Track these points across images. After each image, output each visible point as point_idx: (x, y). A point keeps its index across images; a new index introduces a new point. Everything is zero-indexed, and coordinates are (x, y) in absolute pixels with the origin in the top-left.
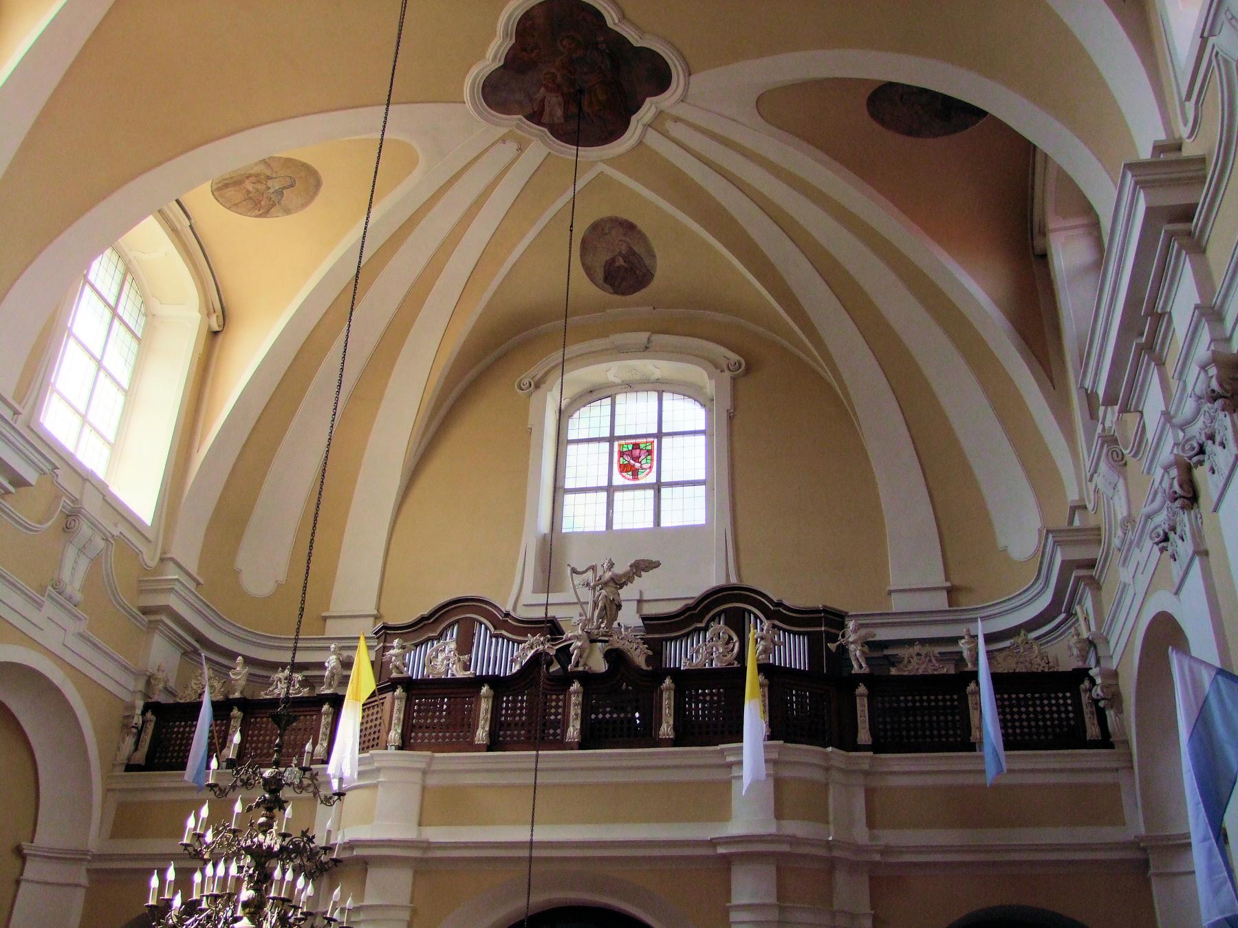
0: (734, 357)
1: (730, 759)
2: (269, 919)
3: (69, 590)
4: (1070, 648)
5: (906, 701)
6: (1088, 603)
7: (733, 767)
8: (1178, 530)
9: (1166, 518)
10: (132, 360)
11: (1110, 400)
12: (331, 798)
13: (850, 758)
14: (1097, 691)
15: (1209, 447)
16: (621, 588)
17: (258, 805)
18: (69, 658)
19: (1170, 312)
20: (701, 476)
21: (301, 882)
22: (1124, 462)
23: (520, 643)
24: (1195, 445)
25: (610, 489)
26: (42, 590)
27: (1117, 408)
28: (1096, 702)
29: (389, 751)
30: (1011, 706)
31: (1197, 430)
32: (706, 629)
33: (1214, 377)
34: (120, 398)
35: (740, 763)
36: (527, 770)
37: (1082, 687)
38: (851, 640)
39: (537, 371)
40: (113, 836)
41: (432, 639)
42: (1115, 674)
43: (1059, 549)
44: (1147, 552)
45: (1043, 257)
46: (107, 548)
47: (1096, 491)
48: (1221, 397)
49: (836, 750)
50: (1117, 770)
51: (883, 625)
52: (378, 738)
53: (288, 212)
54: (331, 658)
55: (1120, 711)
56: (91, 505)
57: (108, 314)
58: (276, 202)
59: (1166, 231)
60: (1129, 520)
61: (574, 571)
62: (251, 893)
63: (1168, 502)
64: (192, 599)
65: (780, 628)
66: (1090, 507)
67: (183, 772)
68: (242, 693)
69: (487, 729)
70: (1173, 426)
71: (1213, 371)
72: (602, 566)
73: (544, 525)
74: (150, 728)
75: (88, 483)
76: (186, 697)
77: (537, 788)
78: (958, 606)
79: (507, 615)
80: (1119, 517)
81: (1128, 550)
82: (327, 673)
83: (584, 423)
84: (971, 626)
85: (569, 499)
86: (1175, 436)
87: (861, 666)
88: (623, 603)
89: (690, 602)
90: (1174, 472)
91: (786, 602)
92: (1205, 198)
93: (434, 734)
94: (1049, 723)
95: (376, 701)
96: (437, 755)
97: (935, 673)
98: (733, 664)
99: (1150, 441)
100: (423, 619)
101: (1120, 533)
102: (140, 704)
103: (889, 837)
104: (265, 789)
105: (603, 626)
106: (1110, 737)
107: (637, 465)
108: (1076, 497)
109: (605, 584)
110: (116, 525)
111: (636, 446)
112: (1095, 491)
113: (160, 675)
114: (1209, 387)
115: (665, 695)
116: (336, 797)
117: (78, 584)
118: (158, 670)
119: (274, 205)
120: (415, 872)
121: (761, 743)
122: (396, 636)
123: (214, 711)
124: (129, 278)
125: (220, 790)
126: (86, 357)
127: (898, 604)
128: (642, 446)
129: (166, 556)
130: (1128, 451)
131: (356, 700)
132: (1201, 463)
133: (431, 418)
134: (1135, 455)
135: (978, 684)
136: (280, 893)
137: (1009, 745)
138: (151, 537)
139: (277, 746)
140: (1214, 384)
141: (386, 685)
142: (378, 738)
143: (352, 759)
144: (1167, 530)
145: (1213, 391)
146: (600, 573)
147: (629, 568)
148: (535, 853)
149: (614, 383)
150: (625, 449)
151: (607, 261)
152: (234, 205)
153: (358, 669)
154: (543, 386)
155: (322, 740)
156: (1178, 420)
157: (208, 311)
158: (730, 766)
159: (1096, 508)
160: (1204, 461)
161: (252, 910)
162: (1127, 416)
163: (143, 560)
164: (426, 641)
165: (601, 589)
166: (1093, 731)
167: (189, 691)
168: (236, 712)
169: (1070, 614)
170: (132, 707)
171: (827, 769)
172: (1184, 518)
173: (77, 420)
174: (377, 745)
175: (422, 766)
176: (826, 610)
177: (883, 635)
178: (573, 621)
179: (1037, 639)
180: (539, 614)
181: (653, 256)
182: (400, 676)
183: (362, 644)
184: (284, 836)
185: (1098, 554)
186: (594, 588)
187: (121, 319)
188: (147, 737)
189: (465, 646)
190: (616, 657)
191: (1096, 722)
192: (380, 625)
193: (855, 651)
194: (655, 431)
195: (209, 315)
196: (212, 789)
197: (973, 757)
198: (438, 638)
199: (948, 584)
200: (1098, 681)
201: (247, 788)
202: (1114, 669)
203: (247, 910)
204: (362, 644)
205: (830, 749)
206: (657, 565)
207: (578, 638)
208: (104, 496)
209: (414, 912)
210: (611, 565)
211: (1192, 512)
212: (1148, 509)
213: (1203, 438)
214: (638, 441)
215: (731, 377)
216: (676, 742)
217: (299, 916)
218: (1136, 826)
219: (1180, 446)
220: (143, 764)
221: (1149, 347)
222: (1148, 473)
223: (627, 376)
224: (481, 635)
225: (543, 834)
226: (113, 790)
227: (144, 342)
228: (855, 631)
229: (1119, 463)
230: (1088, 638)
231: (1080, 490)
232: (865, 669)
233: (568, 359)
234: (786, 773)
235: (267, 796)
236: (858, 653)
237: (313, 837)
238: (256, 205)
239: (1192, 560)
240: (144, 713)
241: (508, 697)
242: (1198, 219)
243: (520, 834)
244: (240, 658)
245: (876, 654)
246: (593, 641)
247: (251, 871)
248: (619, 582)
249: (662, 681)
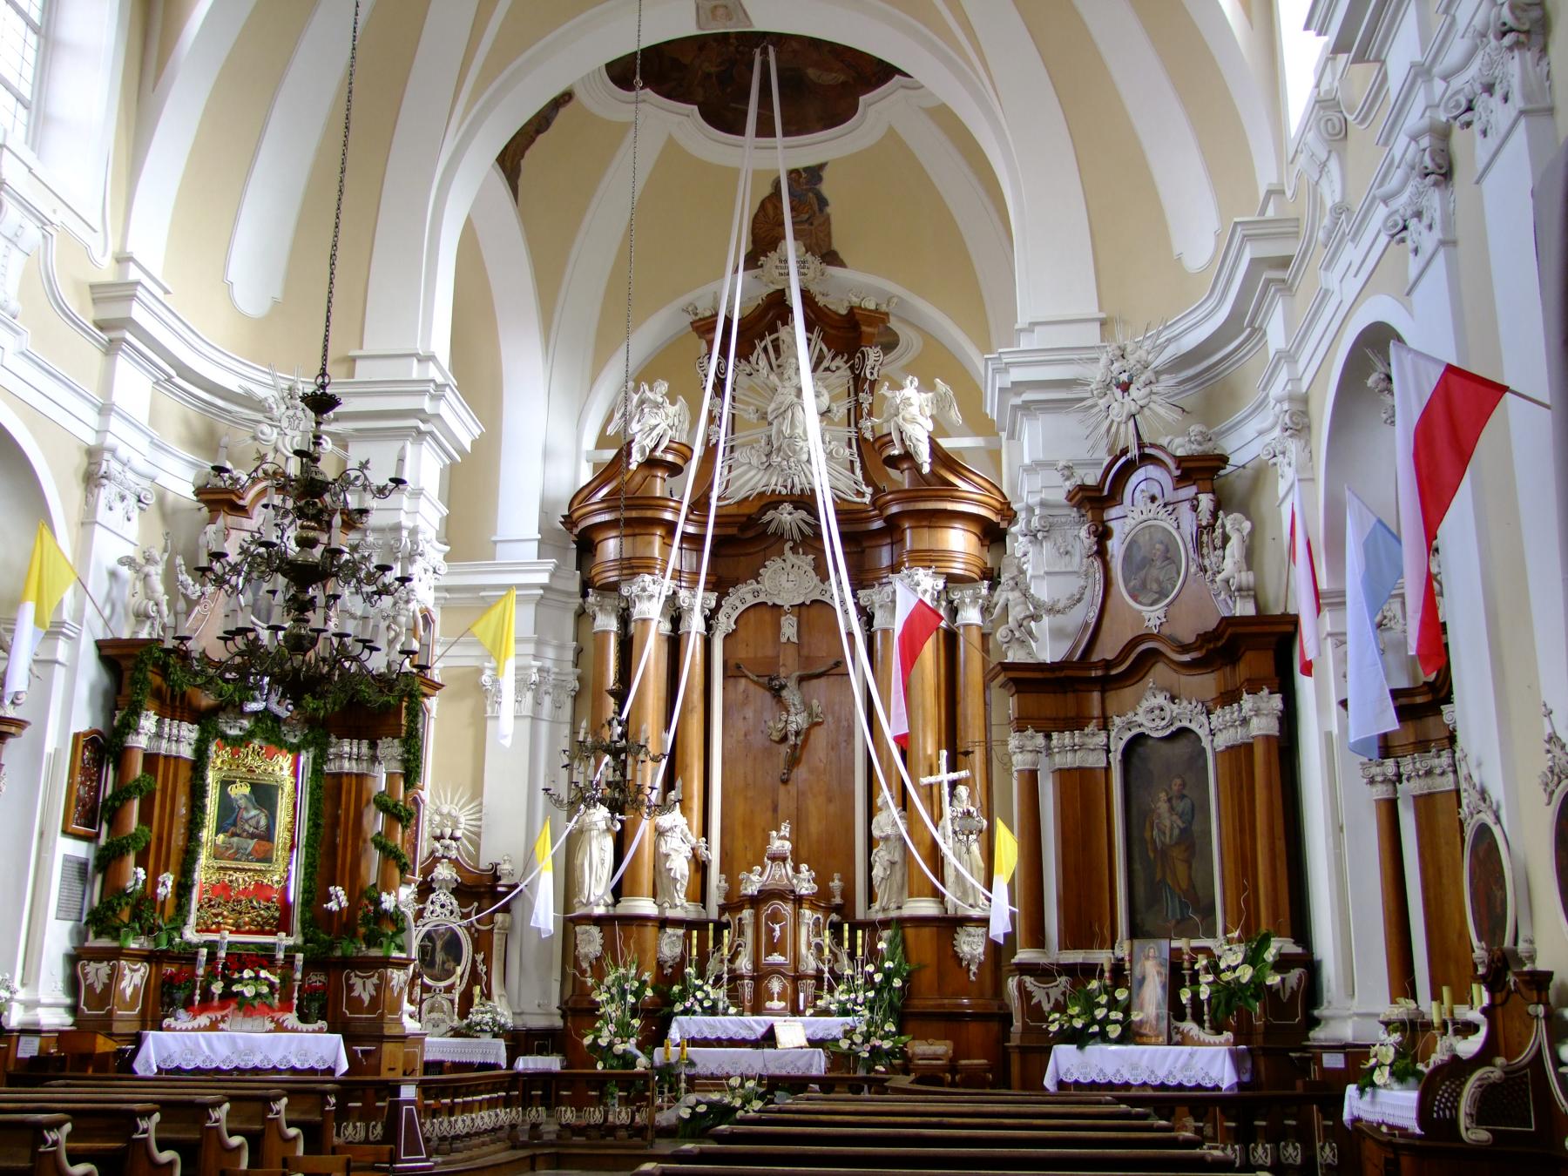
60: (1341, 210)
66: (1289, 194)
80: (1329, 204)
86: (1429, 92)
99: (1393, 101)
108: (1275, 181)
114: (1499, 18)
145: (1504, 24)
172: (1434, 200)
199: (1103, 315)
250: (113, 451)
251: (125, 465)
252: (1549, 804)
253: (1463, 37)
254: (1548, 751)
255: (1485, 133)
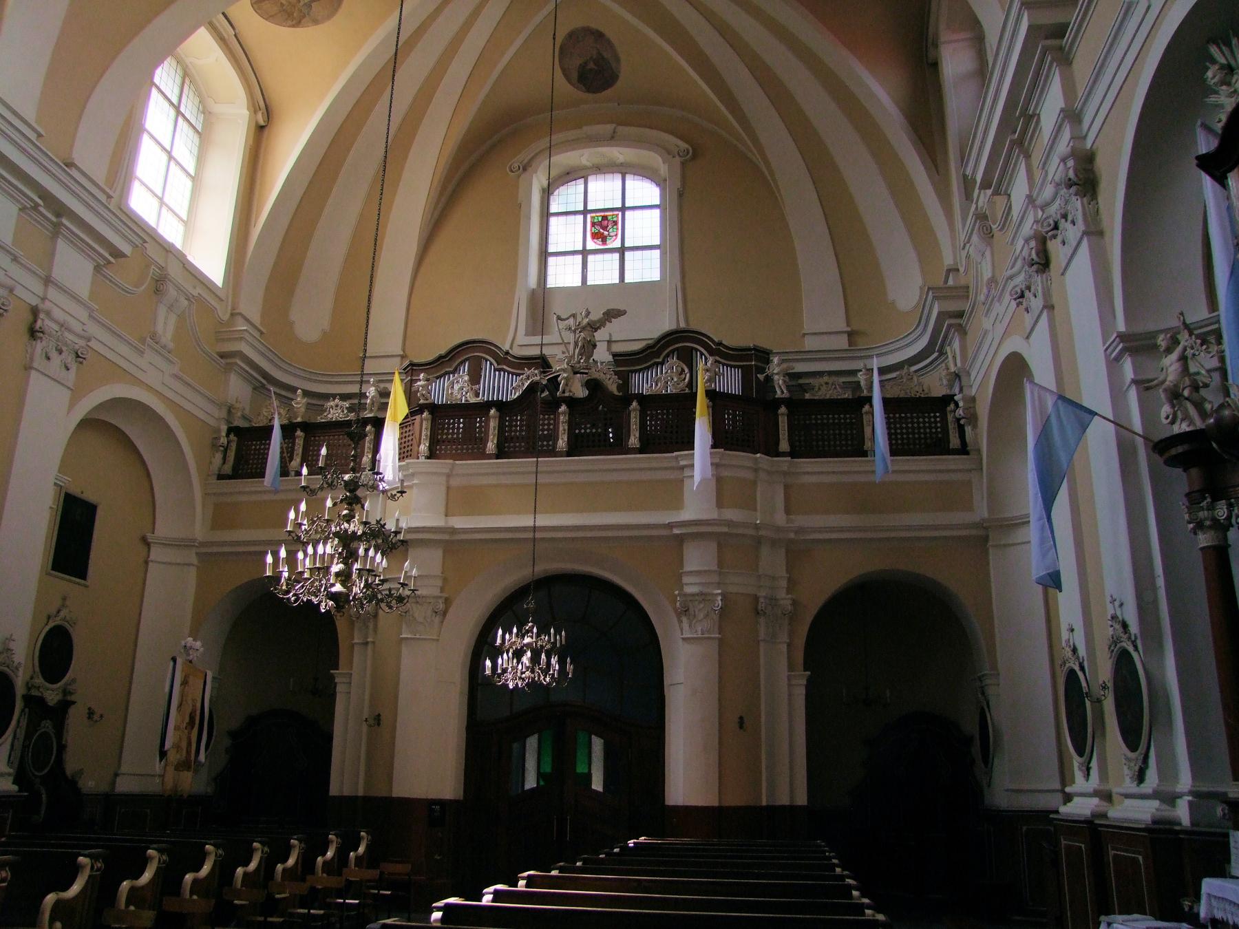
0: (683, 145)
1: (683, 463)
2: (358, 585)
3: (163, 341)
4: (941, 379)
5: (834, 419)
6: (956, 344)
7: (685, 470)
8: (1032, 289)
9: (1024, 279)
10: (195, 150)
11: (986, 185)
12: (395, 495)
13: (774, 461)
14: (960, 412)
15: (1062, 224)
16: (596, 331)
17: (342, 501)
18: (170, 395)
19: (1039, 114)
20: (657, 242)
21: (379, 557)
22: (991, 234)
23: (518, 375)
24: (1052, 222)
25: (585, 253)
26: (143, 340)
27: (989, 192)
28: (958, 420)
29: (420, 460)
30: (895, 423)
31: (1054, 209)
32: (662, 363)
33: (1071, 169)
34: (189, 184)
35: (693, 466)
36: (529, 473)
37: (949, 409)
38: (775, 372)
39: (524, 156)
40: (213, 528)
41: (448, 373)
42: (973, 399)
43: (936, 302)
44: (1007, 304)
45: (935, 66)
46: (190, 305)
47: (968, 257)
48: (1076, 184)
49: (763, 456)
50: (970, 471)
51: (797, 360)
52: (411, 450)
53: (316, 22)
54: (371, 389)
55: (975, 427)
56: (174, 271)
57: (172, 113)
58: (306, 14)
59: (1043, 47)
60: (993, 280)
61: (559, 318)
62: (341, 566)
63: (1027, 267)
64: (256, 344)
65: (720, 362)
66: (962, 270)
67: (263, 479)
68: (302, 418)
69: (495, 442)
70: (1035, 207)
71: (1071, 163)
72: (581, 314)
73: (533, 281)
74: (234, 446)
75: (170, 253)
76: (260, 422)
77: (538, 487)
78: (856, 346)
79: (507, 353)
80: (985, 279)
81: (990, 305)
82: (368, 401)
83: (562, 199)
84: (867, 362)
85: (551, 260)
86: (1035, 216)
87: (782, 392)
88: (597, 343)
89: (650, 342)
90: (1033, 244)
91: (724, 342)
92: (1076, 19)
93: (454, 447)
94: (922, 436)
95: (409, 421)
96: (457, 462)
97: (839, 397)
98: (685, 390)
99: (1015, 221)
100: (441, 357)
101: (985, 290)
102: (224, 428)
103: (801, 521)
104: (345, 489)
105: (582, 361)
106: (967, 447)
107: (606, 233)
109: (583, 329)
110: (195, 288)
111: (605, 218)
112: (966, 257)
113: (237, 405)
114: (1067, 176)
115: (632, 415)
116: (400, 494)
117: (169, 335)
118: (237, 402)
119: (304, 17)
120: (444, 552)
121: (708, 450)
122: (422, 371)
123: (282, 432)
124: (187, 81)
125: (311, 490)
126: (158, 149)
127: (810, 344)
128: (609, 218)
129: (234, 311)
130: (995, 226)
131: (395, 421)
132: (1055, 237)
133: (441, 194)
134: (1000, 230)
135: (871, 406)
136: (315, 564)
137: (893, 453)
138: (222, 296)
139: (353, 456)
140: (1071, 174)
141: (416, 409)
142: (411, 450)
143: (394, 467)
144: (1024, 289)
145: (1070, 179)
146: (579, 319)
147: (602, 316)
148: (538, 535)
149: (586, 166)
150: (596, 221)
151: (580, 65)
152: (271, 16)
153: (395, 399)
154: (530, 169)
155: (368, 452)
156: (1038, 202)
157: (254, 108)
158: (682, 468)
159: (966, 271)
160: (1057, 235)
161: (343, 578)
162: (997, 198)
163: (218, 316)
164: (443, 375)
165: (580, 332)
166: (955, 442)
167: (261, 417)
168: (299, 433)
169: (942, 353)
170: (218, 431)
171: (756, 470)
172: (1038, 280)
173: (156, 203)
174: (411, 456)
175: (447, 471)
176: (756, 349)
177: (800, 368)
178: (557, 357)
179: (916, 371)
180: (535, 352)
181: (618, 60)
182: (426, 402)
183: (397, 378)
184: (365, 523)
185: (967, 307)
186: (575, 331)
187: (183, 116)
188: (232, 455)
189: (475, 378)
190: (594, 386)
191: (957, 435)
192: (407, 363)
193: (779, 381)
194: (620, 205)
195: (255, 112)
196: (304, 490)
197: (866, 461)
198: (453, 372)
199: (849, 329)
200: (961, 404)
201: (332, 489)
202: (973, 395)
203: (339, 579)
204: (397, 378)
205: (758, 455)
206: (624, 313)
207: (564, 370)
208: (184, 264)
209: (445, 580)
210: (588, 313)
211: (1044, 275)
212: (1010, 272)
213: (1059, 217)
214: (607, 214)
215: (681, 162)
216: (642, 450)
217: (377, 582)
218: (981, 511)
219: (1040, 224)
220: (231, 474)
221: (1020, 142)
222: (1012, 244)
223: (597, 160)
224: (487, 368)
225: (544, 520)
226: (209, 494)
227: (204, 136)
228: (779, 365)
229: (988, 235)
230: (955, 372)
231: (955, 258)
232: (786, 394)
233: (554, 146)
234: (726, 473)
235: (348, 494)
236: (781, 382)
237: (385, 524)
238: (289, 16)
239: (1041, 312)
240: (228, 435)
241: (481, 418)
242: (1069, 37)
243: (526, 521)
244: (299, 391)
245: (794, 383)
246: (575, 373)
247: (340, 550)
248: (594, 327)
249: (630, 404)
250: (48, 313)
251: (62, 326)
252: (1110, 658)
253: (1051, 184)
254: (1112, 626)
255: (1064, 243)
